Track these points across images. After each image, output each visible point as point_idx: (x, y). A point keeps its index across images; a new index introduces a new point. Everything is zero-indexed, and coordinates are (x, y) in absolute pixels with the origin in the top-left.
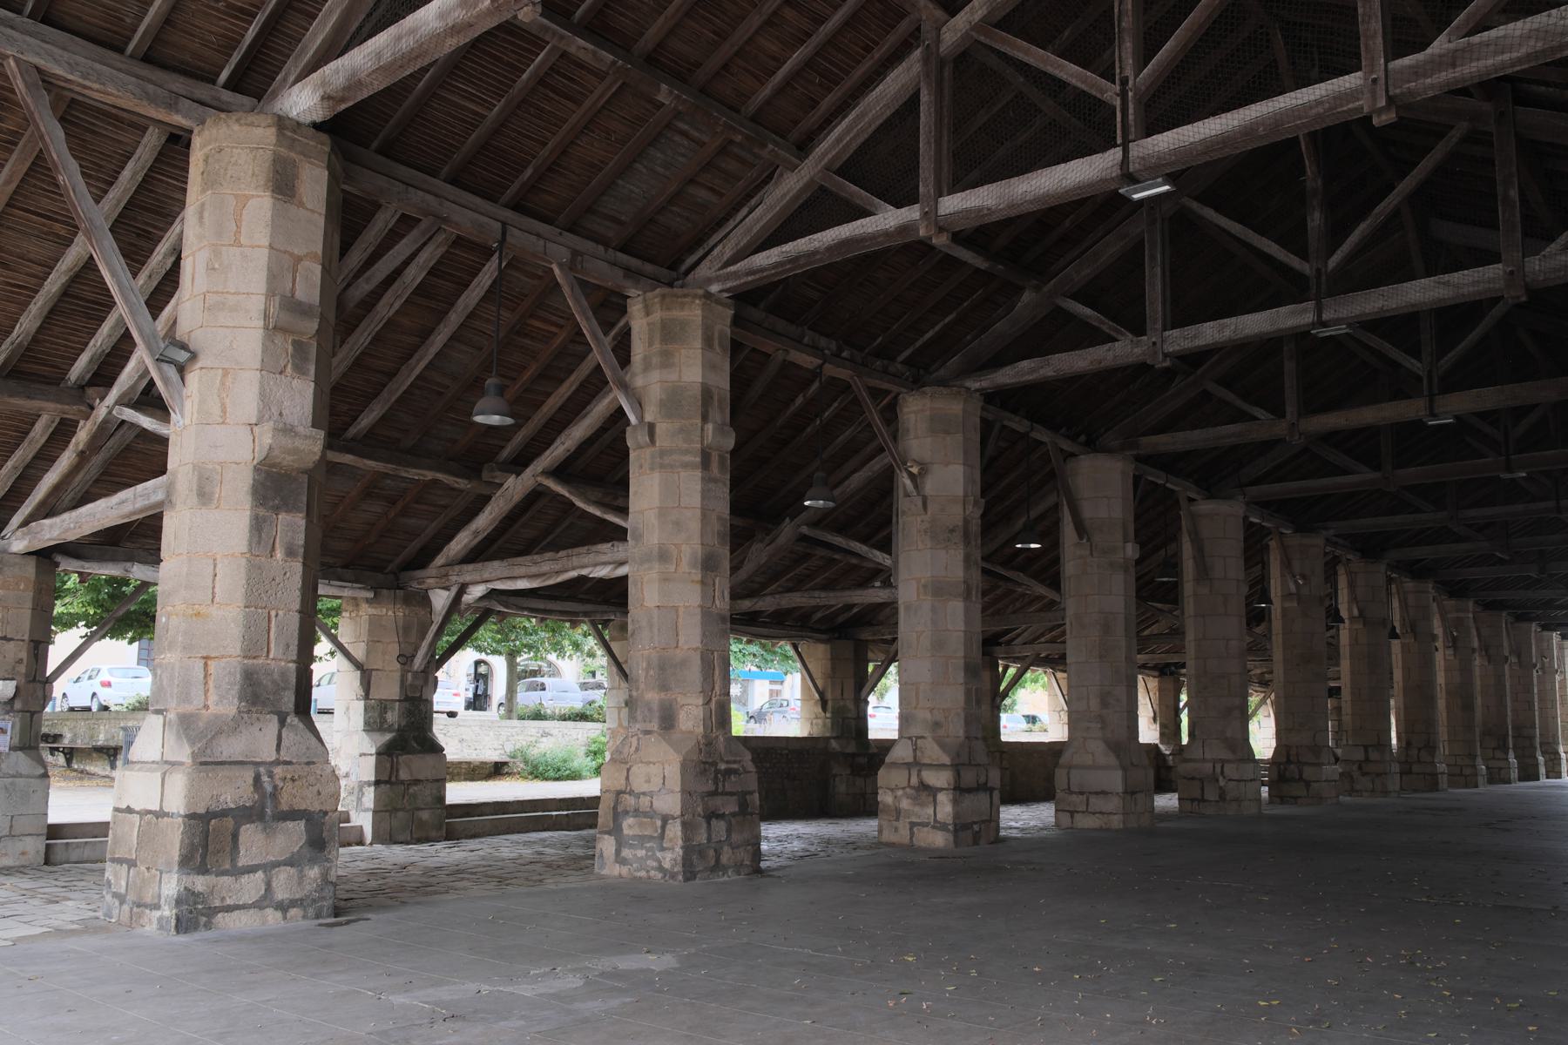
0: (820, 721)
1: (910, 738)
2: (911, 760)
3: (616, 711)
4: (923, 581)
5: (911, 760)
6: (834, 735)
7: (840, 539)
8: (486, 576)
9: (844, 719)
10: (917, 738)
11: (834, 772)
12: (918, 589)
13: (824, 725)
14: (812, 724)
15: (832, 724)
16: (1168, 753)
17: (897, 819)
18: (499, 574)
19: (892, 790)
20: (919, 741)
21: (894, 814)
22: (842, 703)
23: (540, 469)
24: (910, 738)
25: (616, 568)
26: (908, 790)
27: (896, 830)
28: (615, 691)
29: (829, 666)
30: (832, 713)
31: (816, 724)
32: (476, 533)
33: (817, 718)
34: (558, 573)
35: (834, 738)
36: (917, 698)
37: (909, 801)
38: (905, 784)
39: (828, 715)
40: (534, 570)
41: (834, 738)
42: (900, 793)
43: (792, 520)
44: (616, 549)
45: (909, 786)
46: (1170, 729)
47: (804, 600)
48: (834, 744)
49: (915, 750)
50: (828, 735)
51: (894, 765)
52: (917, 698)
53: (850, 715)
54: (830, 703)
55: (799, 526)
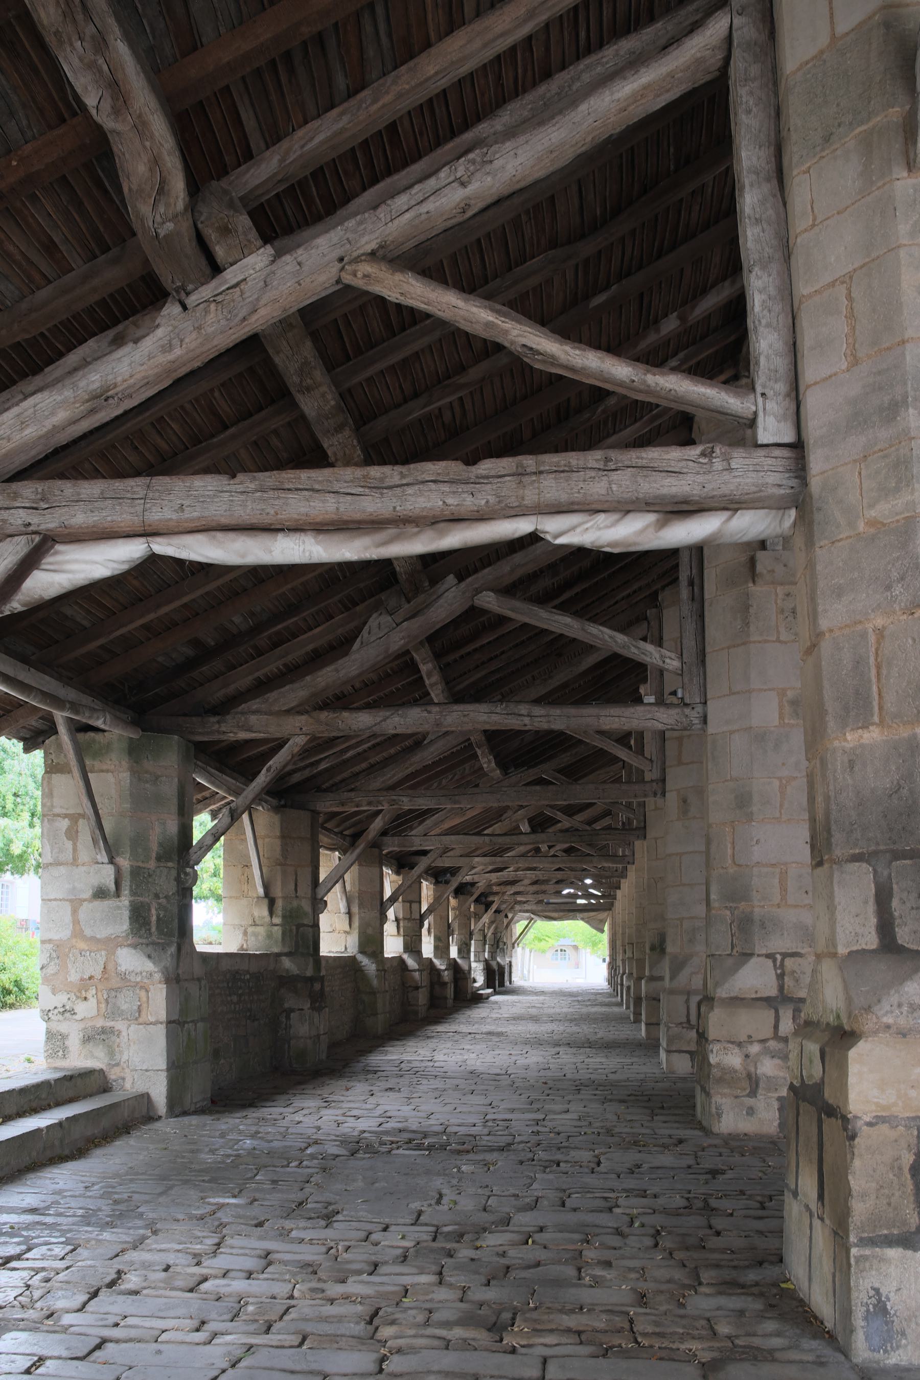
0: (261, 930)
1: (768, 956)
2: (773, 992)
3: (68, 907)
4: (790, 694)
5: (773, 992)
6: (286, 950)
7: (568, 620)
8: (159, 514)
9: (299, 926)
10: (785, 955)
11: (286, 1005)
12: (781, 707)
13: (269, 936)
14: (245, 933)
15: (284, 934)
16: (443, 967)
17: (753, 1093)
18: (218, 510)
19: (740, 1045)
20: (789, 962)
21: (745, 1084)
22: (295, 903)
23: (369, 243)
24: (768, 956)
25: (661, 525)
26: (772, 1044)
27: (751, 1111)
28: (62, 870)
29: (278, 849)
30: (284, 917)
31: (255, 935)
32: (102, 396)
33: (255, 924)
34: (481, 517)
35: (287, 954)
36: (784, 889)
37: (777, 1061)
38: (768, 1032)
39: (277, 920)
40: (348, 508)
41: (287, 954)
42: (755, 1049)
43: (461, 578)
44: (718, 464)
45: (776, 1036)
46: (412, 945)
47: (495, 718)
48: (287, 963)
49: (781, 977)
50: (276, 950)
51: (737, 1002)
52: (784, 889)
53: (306, 922)
54: (279, 904)
55: (478, 591)
